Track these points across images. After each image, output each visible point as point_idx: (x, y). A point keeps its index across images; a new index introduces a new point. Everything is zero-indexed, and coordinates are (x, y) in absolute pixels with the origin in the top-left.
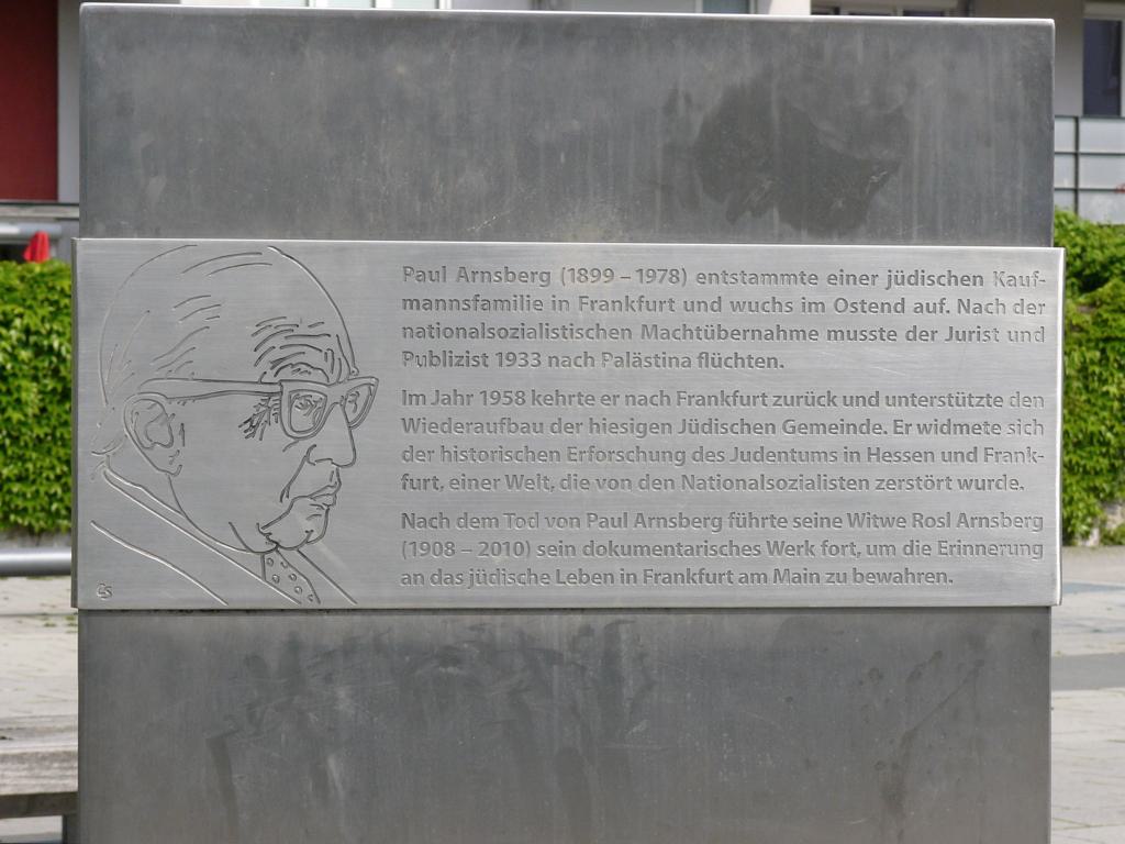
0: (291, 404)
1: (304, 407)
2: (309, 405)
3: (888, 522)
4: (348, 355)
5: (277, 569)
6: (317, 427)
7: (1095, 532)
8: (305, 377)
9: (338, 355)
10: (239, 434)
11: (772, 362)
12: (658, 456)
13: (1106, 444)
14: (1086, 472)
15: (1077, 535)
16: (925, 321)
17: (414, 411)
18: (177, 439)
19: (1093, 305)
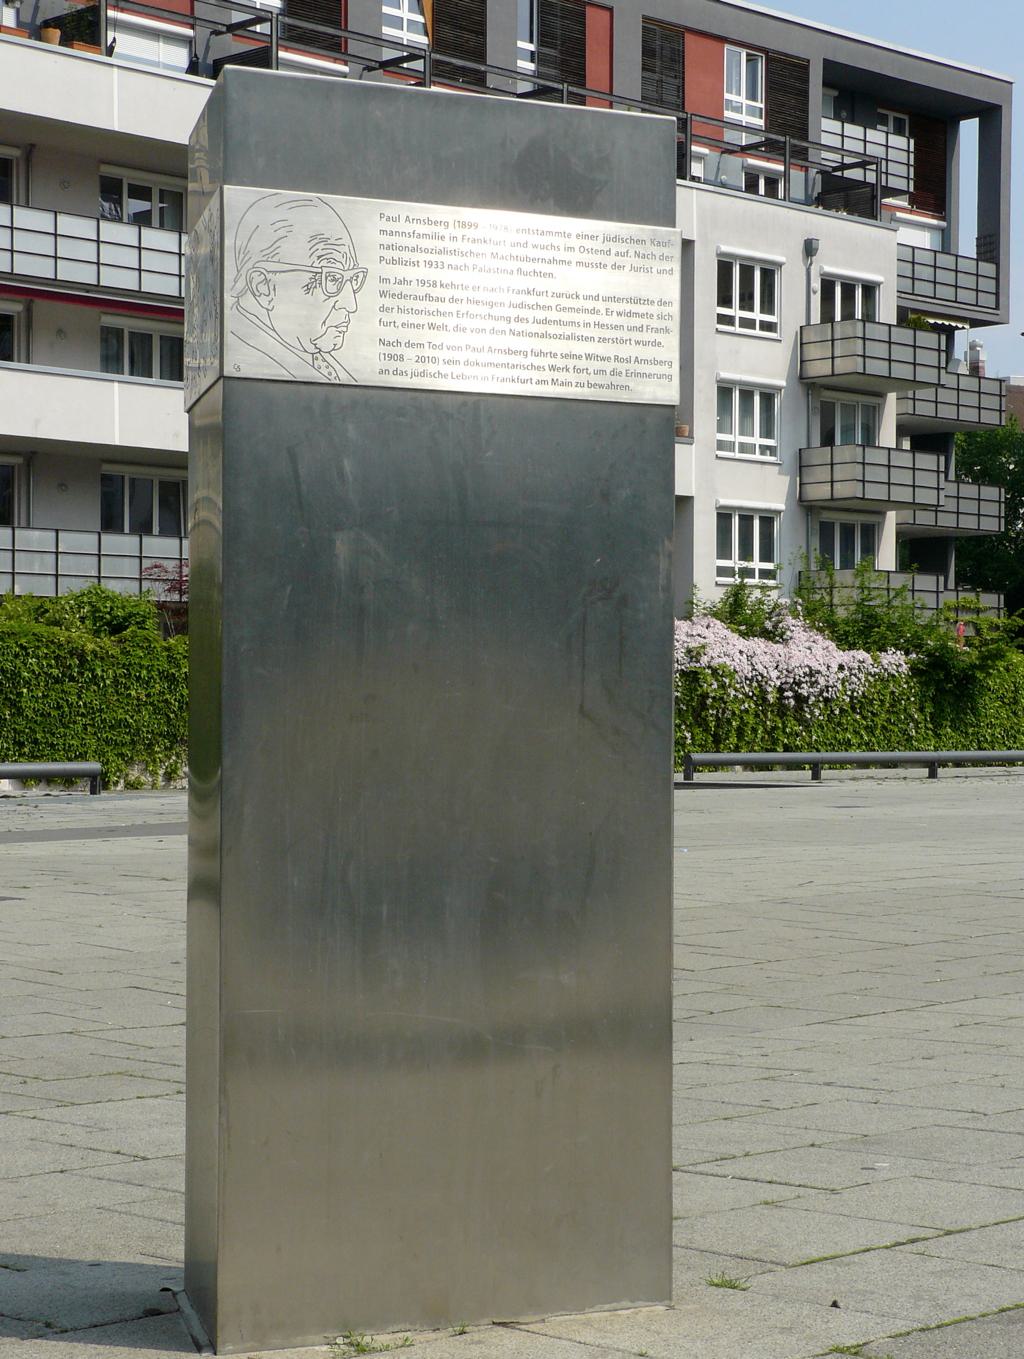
0: (326, 278)
1: (333, 281)
2: (334, 280)
3: (603, 359)
4: (353, 255)
5: (319, 362)
6: (339, 291)
7: (122, 781)
8: (333, 265)
9: (349, 255)
10: (302, 292)
11: (551, 275)
12: (497, 319)
13: (128, 726)
14: (116, 744)
15: (111, 783)
16: (619, 260)
17: (385, 287)
18: (272, 292)
19: (120, 641)
